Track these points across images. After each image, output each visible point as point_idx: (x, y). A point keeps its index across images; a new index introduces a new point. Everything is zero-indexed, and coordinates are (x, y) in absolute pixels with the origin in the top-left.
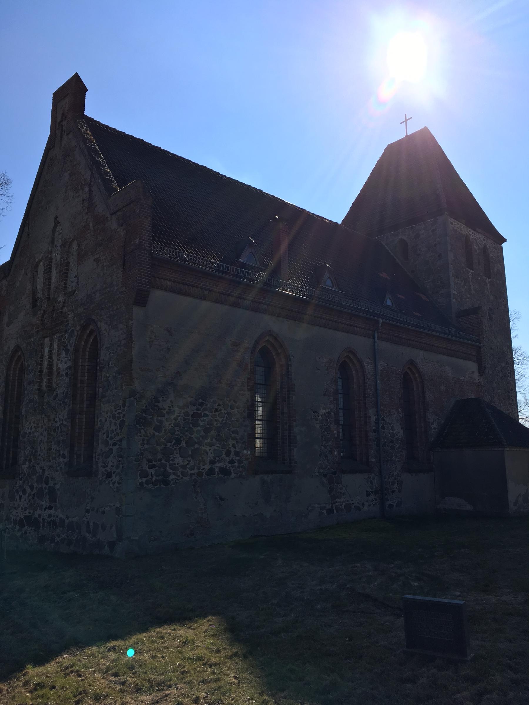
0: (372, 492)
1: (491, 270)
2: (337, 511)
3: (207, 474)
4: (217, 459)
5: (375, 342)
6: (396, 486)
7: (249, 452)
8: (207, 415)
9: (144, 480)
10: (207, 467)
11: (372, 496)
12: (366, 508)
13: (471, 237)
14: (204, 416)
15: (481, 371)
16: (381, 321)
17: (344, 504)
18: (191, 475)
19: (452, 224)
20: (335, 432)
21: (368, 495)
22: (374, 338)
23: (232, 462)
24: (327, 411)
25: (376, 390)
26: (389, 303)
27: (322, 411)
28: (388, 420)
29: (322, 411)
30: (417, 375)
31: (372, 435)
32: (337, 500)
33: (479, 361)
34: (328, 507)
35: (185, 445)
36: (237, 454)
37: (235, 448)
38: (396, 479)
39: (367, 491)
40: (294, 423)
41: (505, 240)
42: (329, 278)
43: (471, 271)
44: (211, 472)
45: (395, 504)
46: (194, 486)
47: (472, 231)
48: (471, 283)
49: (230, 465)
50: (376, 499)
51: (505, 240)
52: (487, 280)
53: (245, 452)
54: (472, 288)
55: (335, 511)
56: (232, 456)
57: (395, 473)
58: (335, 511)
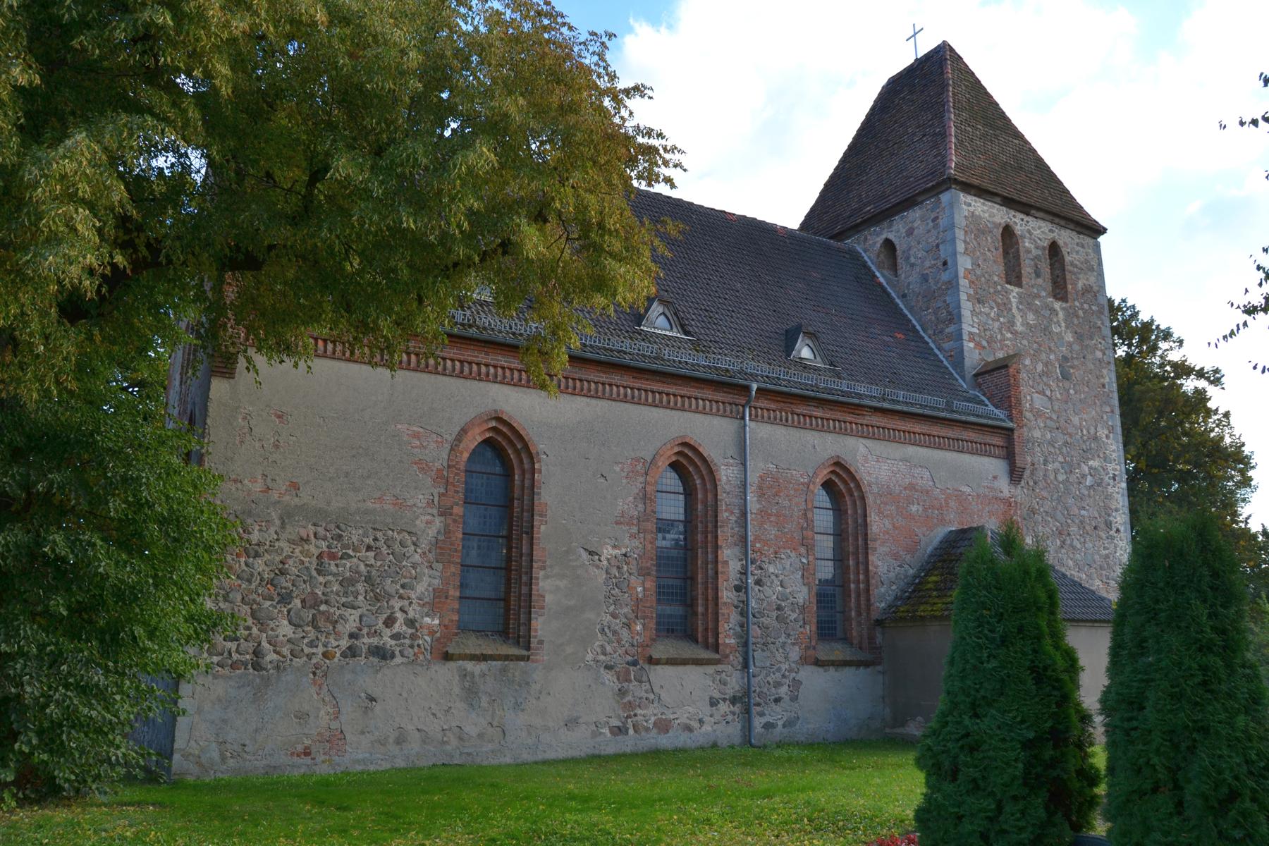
0: (724, 700)
1: (1070, 287)
2: (636, 731)
3: (344, 655)
4: (365, 631)
5: (745, 426)
6: (783, 691)
7: (437, 622)
8: (350, 557)
9: (215, 659)
10: (345, 643)
11: (724, 707)
12: (707, 728)
13: (1018, 227)
14: (341, 558)
15: (1015, 474)
16: (755, 386)
17: (653, 719)
18: (310, 656)
19: (970, 205)
20: (639, 589)
21: (713, 703)
22: (743, 418)
23: (396, 637)
24: (624, 551)
25: (744, 514)
26: (806, 353)
27: (608, 551)
28: (771, 569)
29: (608, 551)
30: (852, 485)
31: (727, 595)
32: (639, 711)
33: (1009, 455)
34: (615, 722)
35: (299, 605)
36: (411, 623)
37: (406, 612)
38: (784, 676)
39: (711, 698)
40: (542, 573)
41: (1102, 231)
42: (663, 313)
43: (1017, 289)
44: (352, 652)
45: (780, 723)
46: (314, 674)
47: (1022, 216)
48: (1014, 310)
49: (393, 642)
50: (733, 713)
51: (1102, 231)
52: (1057, 305)
53: (427, 620)
54: (1019, 321)
55: (631, 731)
56: (399, 627)
57: (784, 667)
58: (631, 731)
